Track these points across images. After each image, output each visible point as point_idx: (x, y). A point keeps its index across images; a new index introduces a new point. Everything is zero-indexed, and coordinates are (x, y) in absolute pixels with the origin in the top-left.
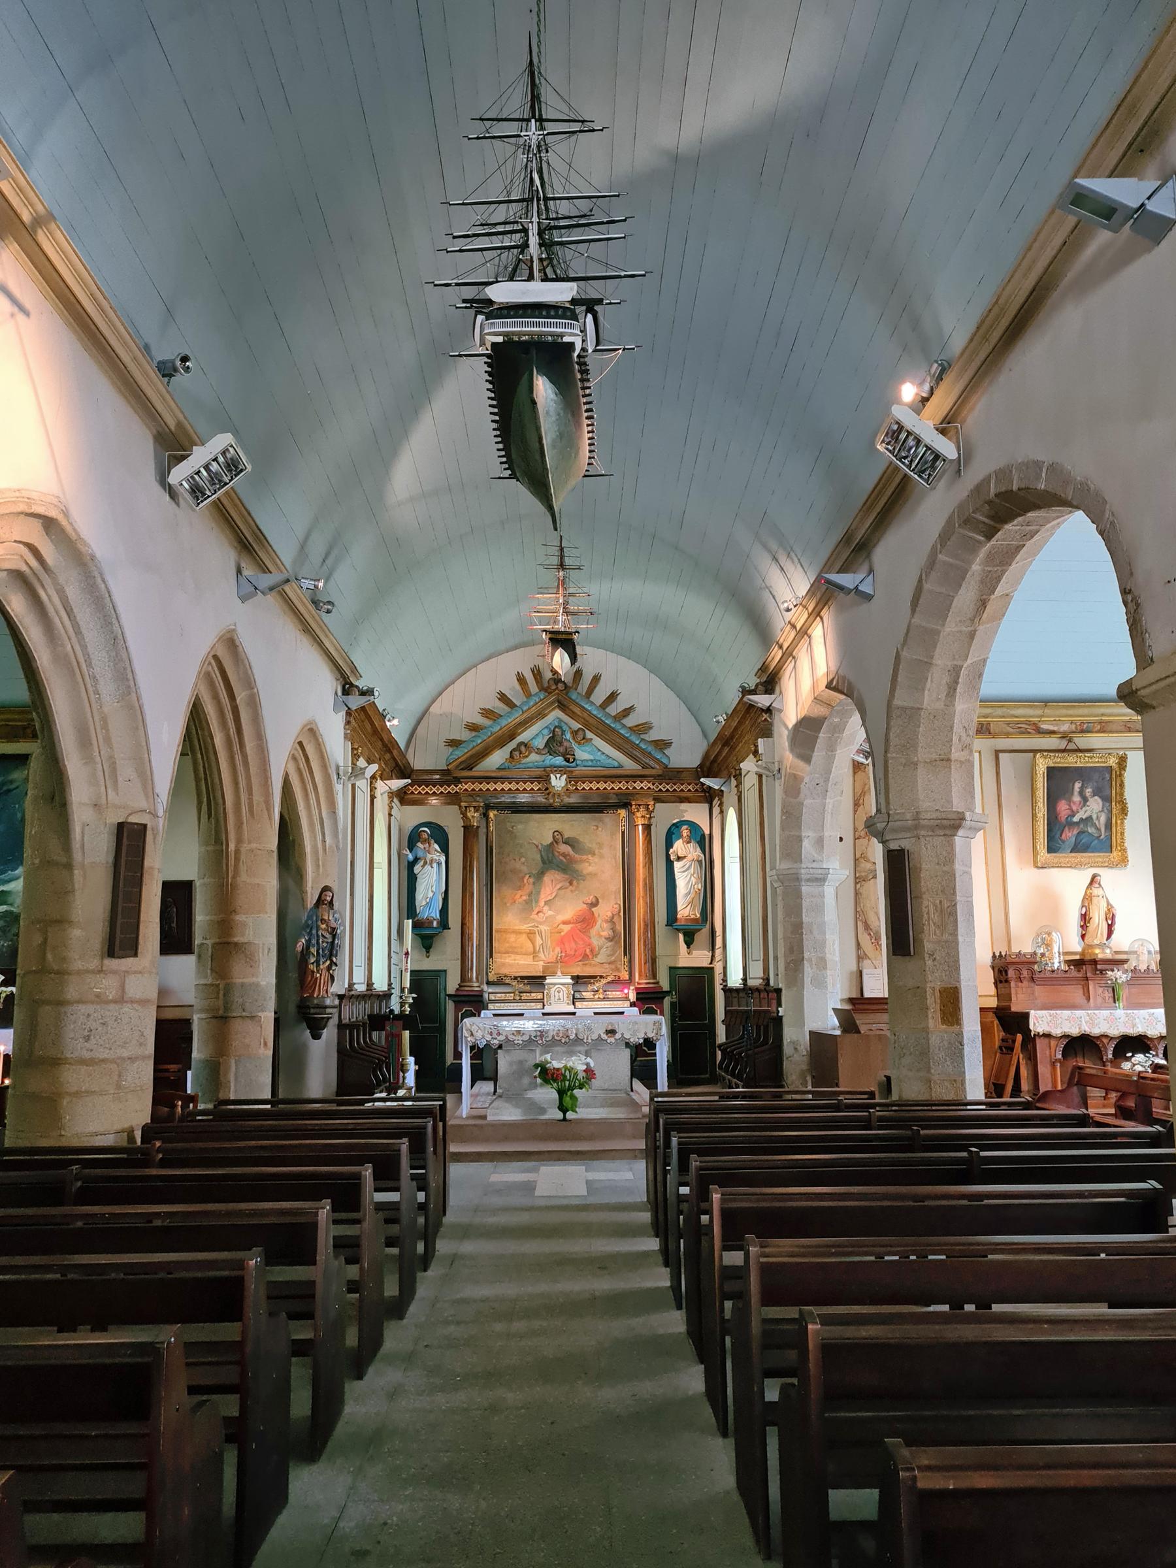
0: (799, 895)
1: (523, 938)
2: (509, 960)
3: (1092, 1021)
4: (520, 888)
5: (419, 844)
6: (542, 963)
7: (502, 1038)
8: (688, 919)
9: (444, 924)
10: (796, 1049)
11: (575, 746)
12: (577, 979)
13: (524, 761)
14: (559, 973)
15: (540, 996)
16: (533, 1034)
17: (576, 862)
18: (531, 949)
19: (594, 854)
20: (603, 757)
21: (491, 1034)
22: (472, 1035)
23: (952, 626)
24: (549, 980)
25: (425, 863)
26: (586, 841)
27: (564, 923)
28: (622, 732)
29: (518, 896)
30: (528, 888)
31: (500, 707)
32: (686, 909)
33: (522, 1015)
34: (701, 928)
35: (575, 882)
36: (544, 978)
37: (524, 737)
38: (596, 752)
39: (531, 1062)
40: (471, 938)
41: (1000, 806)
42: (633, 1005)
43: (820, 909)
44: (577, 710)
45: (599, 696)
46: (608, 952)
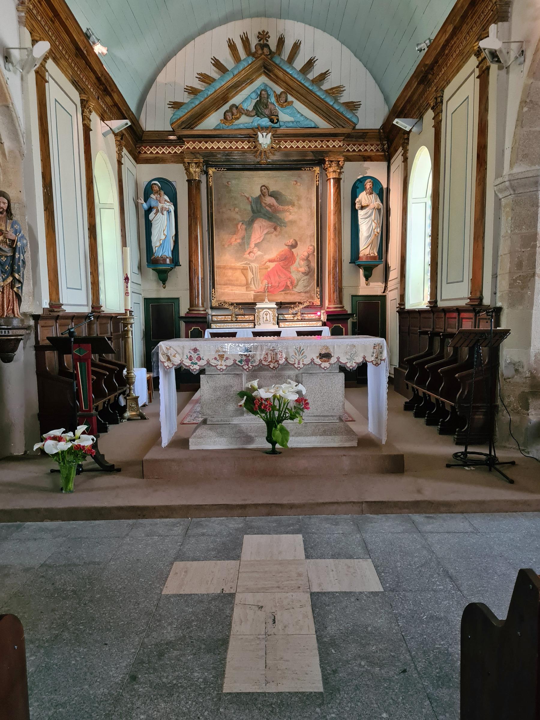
1: (238, 274)
2: (228, 290)
4: (235, 233)
5: (152, 196)
6: (253, 293)
7: (202, 363)
8: (367, 257)
9: (175, 261)
10: (517, 371)
11: (278, 108)
12: (281, 305)
13: (237, 122)
14: (267, 300)
15: (252, 318)
16: (238, 359)
17: (279, 211)
18: (244, 282)
19: (293, 205)
20: (302, 118)
21: (191, 358)
22: (169, 359)
24: (259, 306)
25: (157, 211)
26: (288, 194)
27: (271, 261)
28: (318, 93)
29: (233, 240)
30: (242, 233)
31: (213, 73)
32: (367, 248)
33: (233, 335)
35: (278, 229)
36: (255, 304)
37: (236, 100)
38: (297, 114)
39: (237, 389)
40: (196, 273)
42: (324, 324)
44: (280, 74)
45: (300, 62)
46: (305, 284)
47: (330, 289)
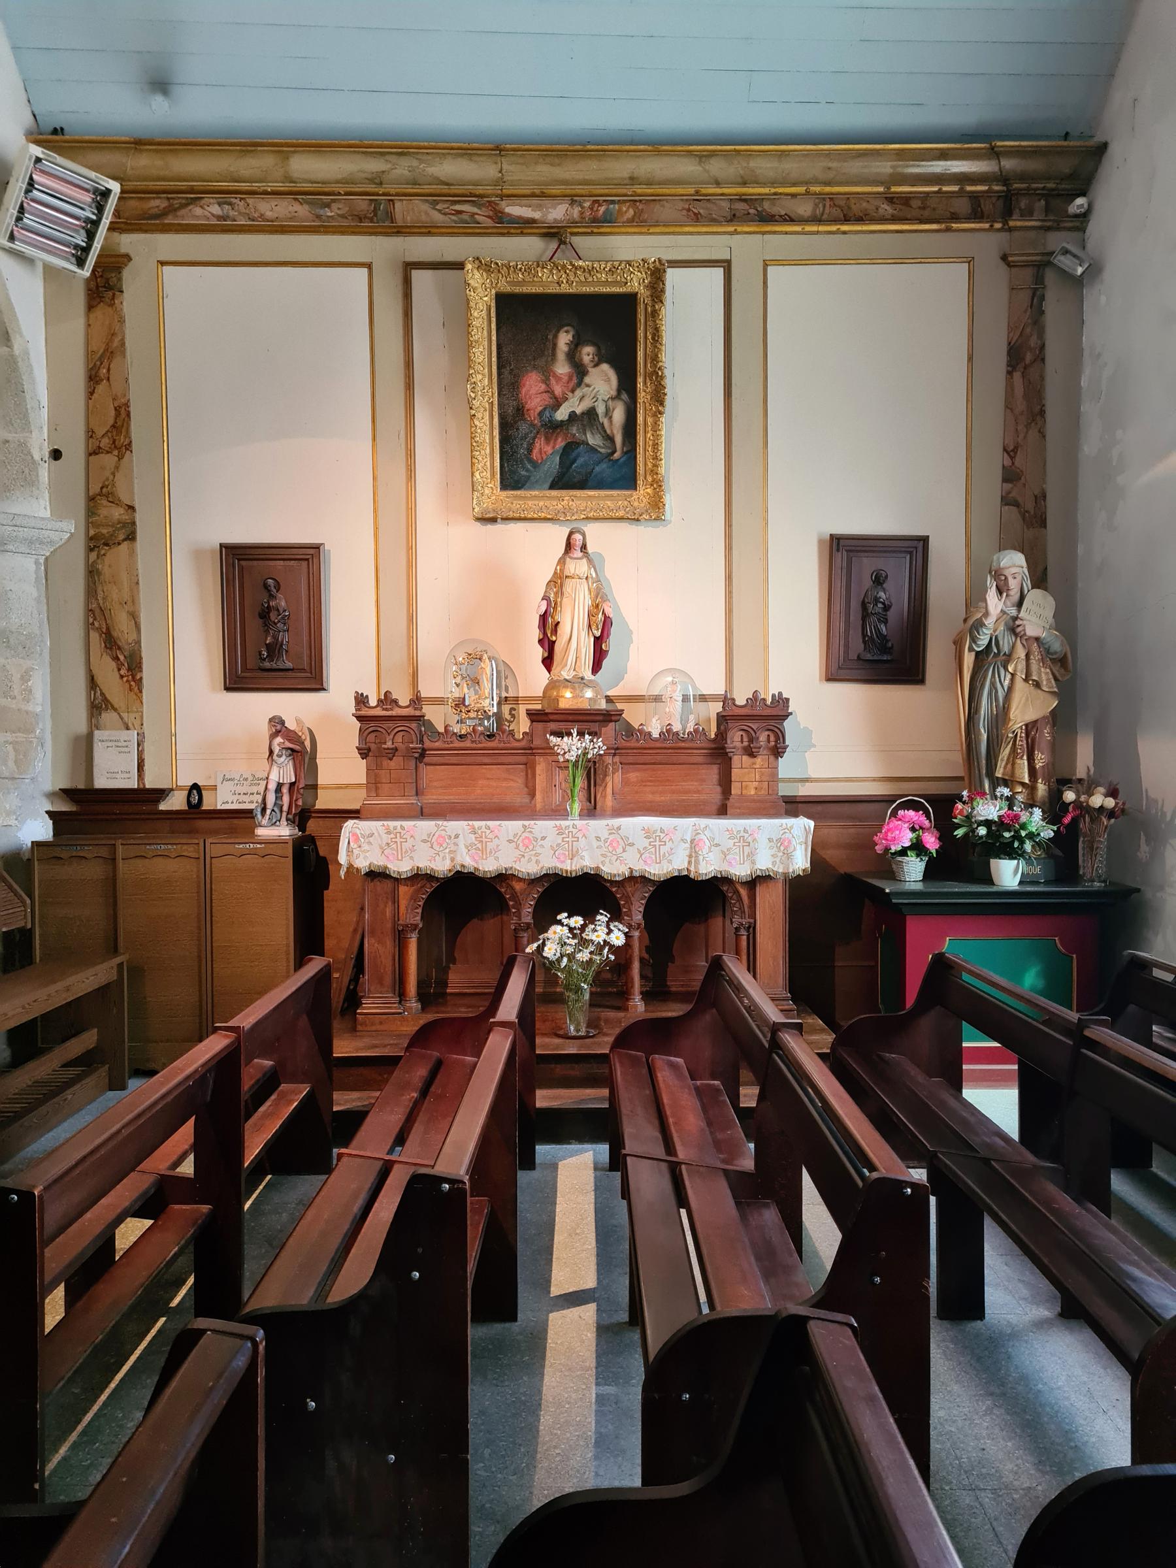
3: (481, 846)
41: (409, 386)
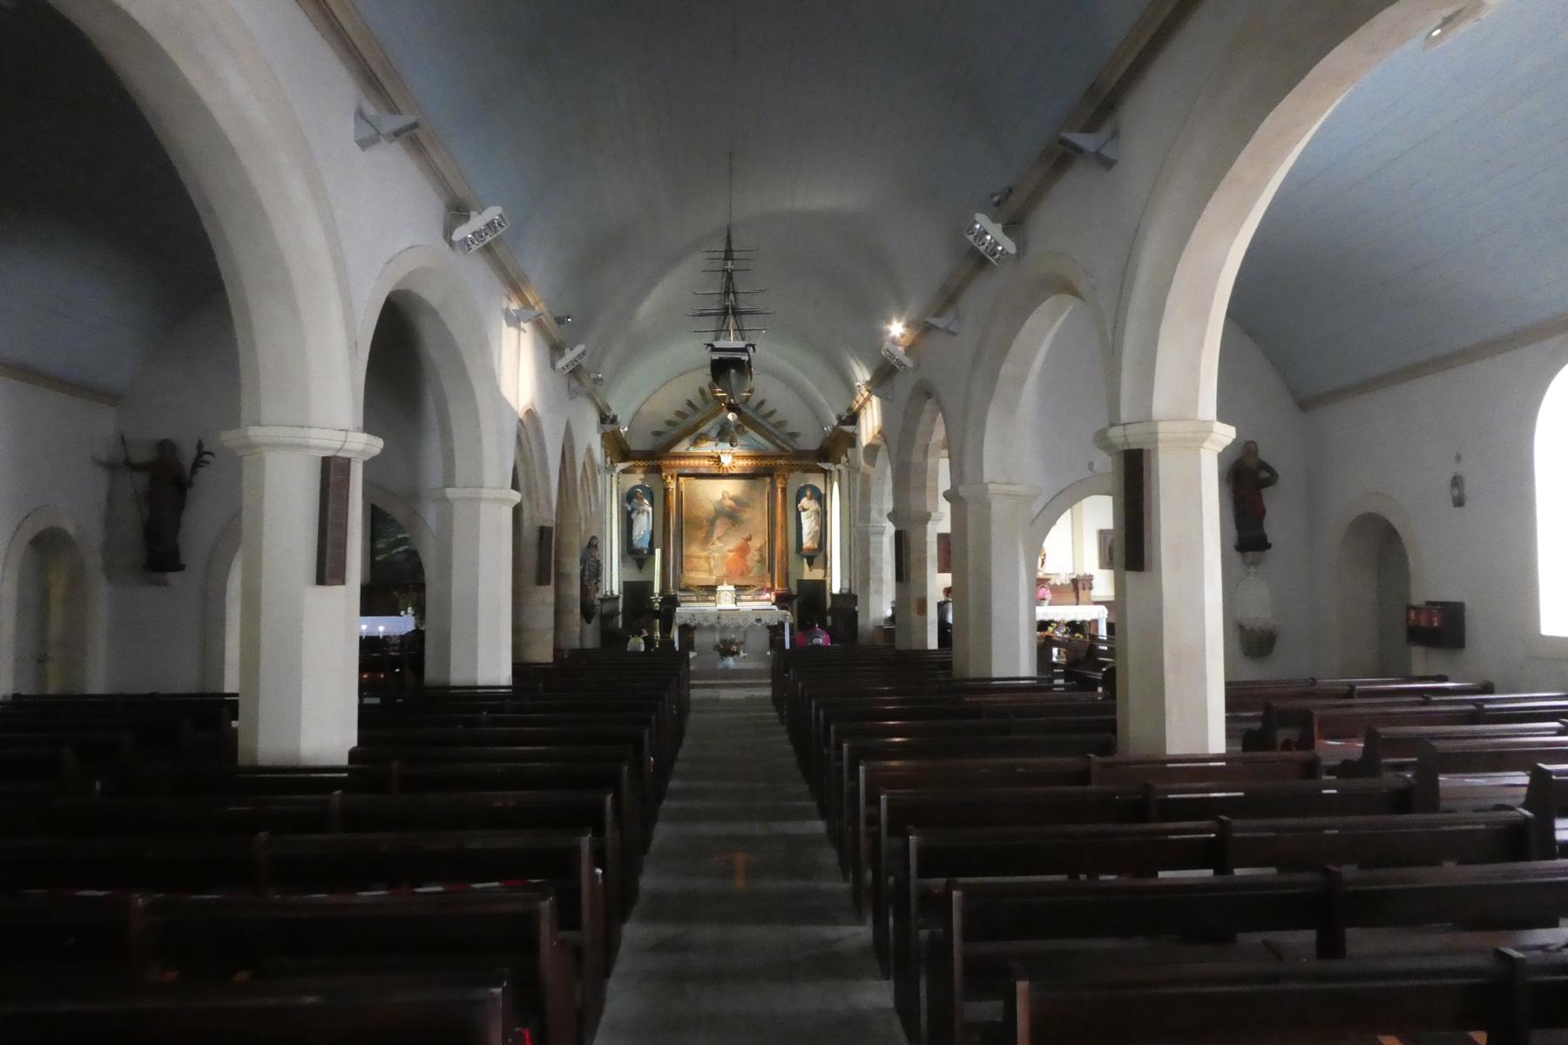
0: (868, 543)
2: (693, 575)
8: (809, 549)
23: (921, 428)
31: (688, 410)
32: (807, 542)
34: (818, 555)
43: (880, 550)
47: (1451, 824)
